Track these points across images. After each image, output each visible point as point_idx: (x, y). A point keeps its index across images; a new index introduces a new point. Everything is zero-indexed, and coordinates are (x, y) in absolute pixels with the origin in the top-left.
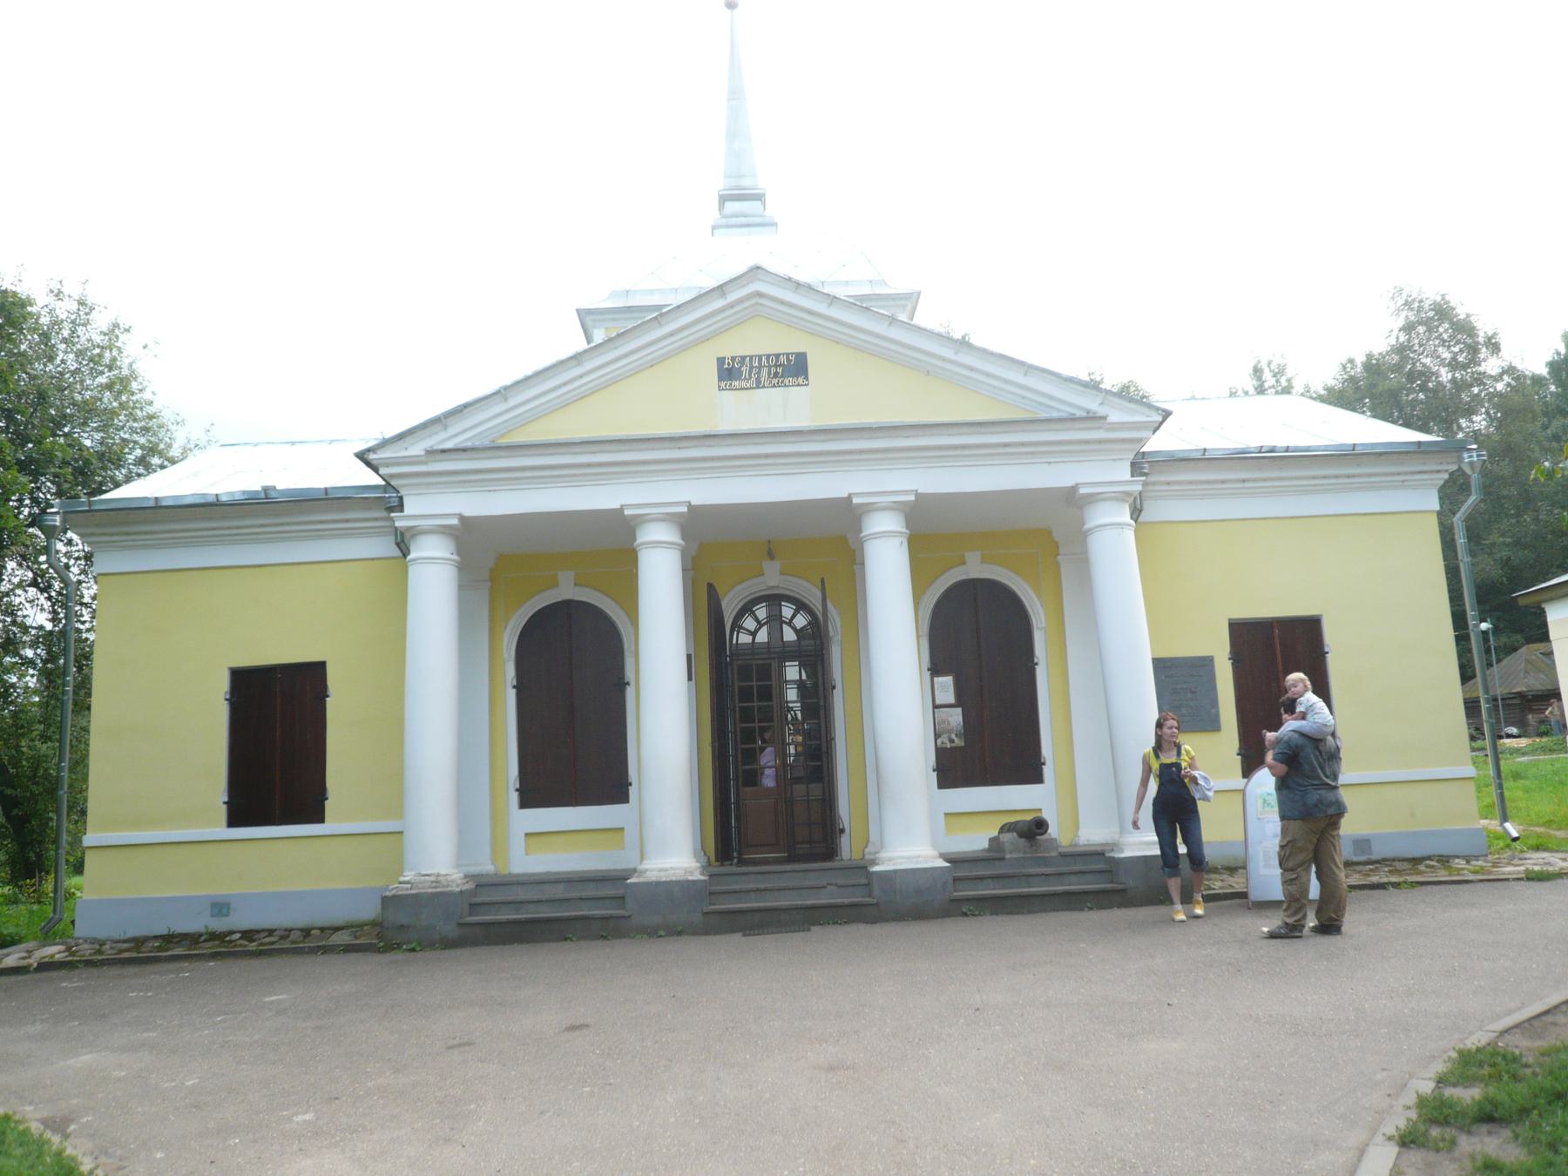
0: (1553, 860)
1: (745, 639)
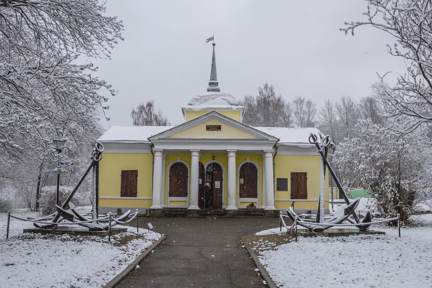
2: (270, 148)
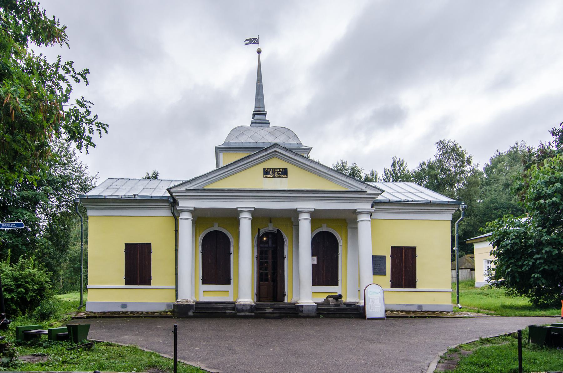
0: (469, 314)
2: (367, 206)
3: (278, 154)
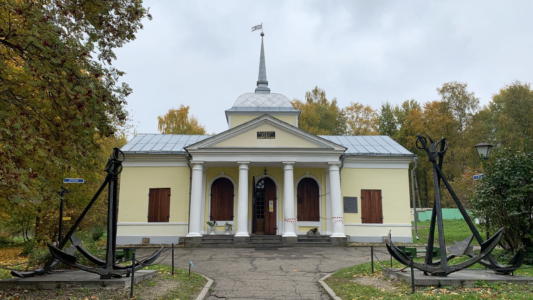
1: (259, 187)
2: (337, 160)
3: (267, 121)
